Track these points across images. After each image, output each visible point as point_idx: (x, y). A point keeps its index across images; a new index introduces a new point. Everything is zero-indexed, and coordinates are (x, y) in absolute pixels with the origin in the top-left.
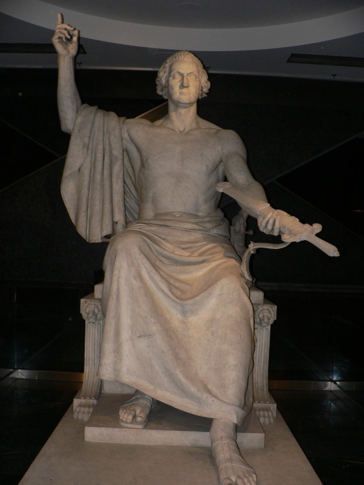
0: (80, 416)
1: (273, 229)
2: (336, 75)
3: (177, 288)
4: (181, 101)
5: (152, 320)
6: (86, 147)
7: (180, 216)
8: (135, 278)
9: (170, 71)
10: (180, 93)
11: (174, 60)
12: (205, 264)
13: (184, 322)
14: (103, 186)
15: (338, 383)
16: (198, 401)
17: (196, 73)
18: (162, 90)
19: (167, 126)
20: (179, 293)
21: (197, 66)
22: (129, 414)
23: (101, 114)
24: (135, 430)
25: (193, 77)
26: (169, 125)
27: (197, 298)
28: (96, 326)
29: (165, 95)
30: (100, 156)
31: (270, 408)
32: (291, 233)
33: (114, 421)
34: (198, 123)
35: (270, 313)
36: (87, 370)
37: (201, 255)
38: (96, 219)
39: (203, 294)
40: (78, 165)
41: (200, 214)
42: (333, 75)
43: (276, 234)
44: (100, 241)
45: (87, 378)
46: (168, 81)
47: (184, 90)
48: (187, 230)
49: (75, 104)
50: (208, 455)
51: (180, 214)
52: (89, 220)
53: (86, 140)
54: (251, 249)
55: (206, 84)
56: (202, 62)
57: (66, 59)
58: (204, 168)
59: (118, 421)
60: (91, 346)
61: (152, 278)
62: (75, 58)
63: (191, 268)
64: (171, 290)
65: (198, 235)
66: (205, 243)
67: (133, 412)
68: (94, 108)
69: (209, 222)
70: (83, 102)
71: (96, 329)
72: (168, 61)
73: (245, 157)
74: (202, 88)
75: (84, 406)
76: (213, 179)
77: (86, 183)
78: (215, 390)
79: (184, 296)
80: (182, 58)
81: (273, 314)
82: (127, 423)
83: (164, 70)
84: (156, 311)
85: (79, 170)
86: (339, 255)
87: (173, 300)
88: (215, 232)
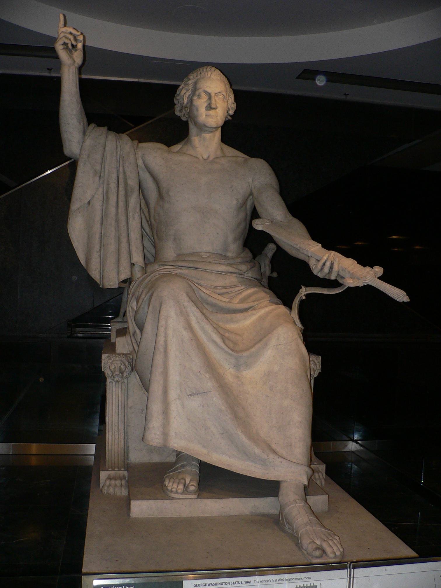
0: (111, 490)
1: (330, 272)
2: (348, 94)
3: (228, 339)
4: (208, 125)
5: (207, 375)
6: (99, 174)
7: (208, 257)
8: (185, 329)
9: (195, 89)
10: (206, 115)
11: (199, 77)
12: (250, 313)
13: (238, 377)
14: (118, 222)
15: (359, 442)
16: (264, 463)
17: (224, 93)
18: (181, 111)
19: (188, 153)
20: (232, 345)
21: (225, 84)
22: (179, 483)
23: (112, 136)
24: (188, 500)
25: (221, 97)
26: (191, 152)
27: (253, 350)
28: (120, 385)
29: (184, 116)
30: (113, 186)
31: (318, 469)
32: (353, 276)
33: (160, 492)
34: (222, 150)
35: (316, 365)
36: (110, 438)
37: (242, 301)
38: (111, 262)
39: (259, 345)
40: (88, 197)
41: (229, 254)
42: (345, 94)
43: (333, 278)
44: (117, 286)
45: (110, 447)
46: (191, 101)
47: (212, 112)
48: (221, 273)
49: (82, 124)
50: (277, 521)
51: (208, 255)
52: (102, 264)
53: (98, 167)
54: (303, 294)
55: (233, 106)
56: (228, 80)
57: (71, 70)
58: (235, 202)
59: (164, 491)
60: (114, 408)
61: (203, 329)
62: (80, 70)
63: (239, 316)
64: (224, 342)
65: (233, 279)
66: (243, 287)
67: (183, 481)
68: (104, 129)
69: (241, 263)
70: (89, 123)
71: (120, 389)
72: (191, 77)
73: (278, 189)
74: (228, 109)
75: (115, 478)
76: (242, 215)
77: (98, 218)
78: (280, 450)
79: (241, 350)
80: (209, 75)
81: (318, 366)
82: (177, 493)
83: (186, 88)
84: (210, 366)
85: (89, 203)
86: (409, 300)
87: (226, 352)
88: (249, 274)
